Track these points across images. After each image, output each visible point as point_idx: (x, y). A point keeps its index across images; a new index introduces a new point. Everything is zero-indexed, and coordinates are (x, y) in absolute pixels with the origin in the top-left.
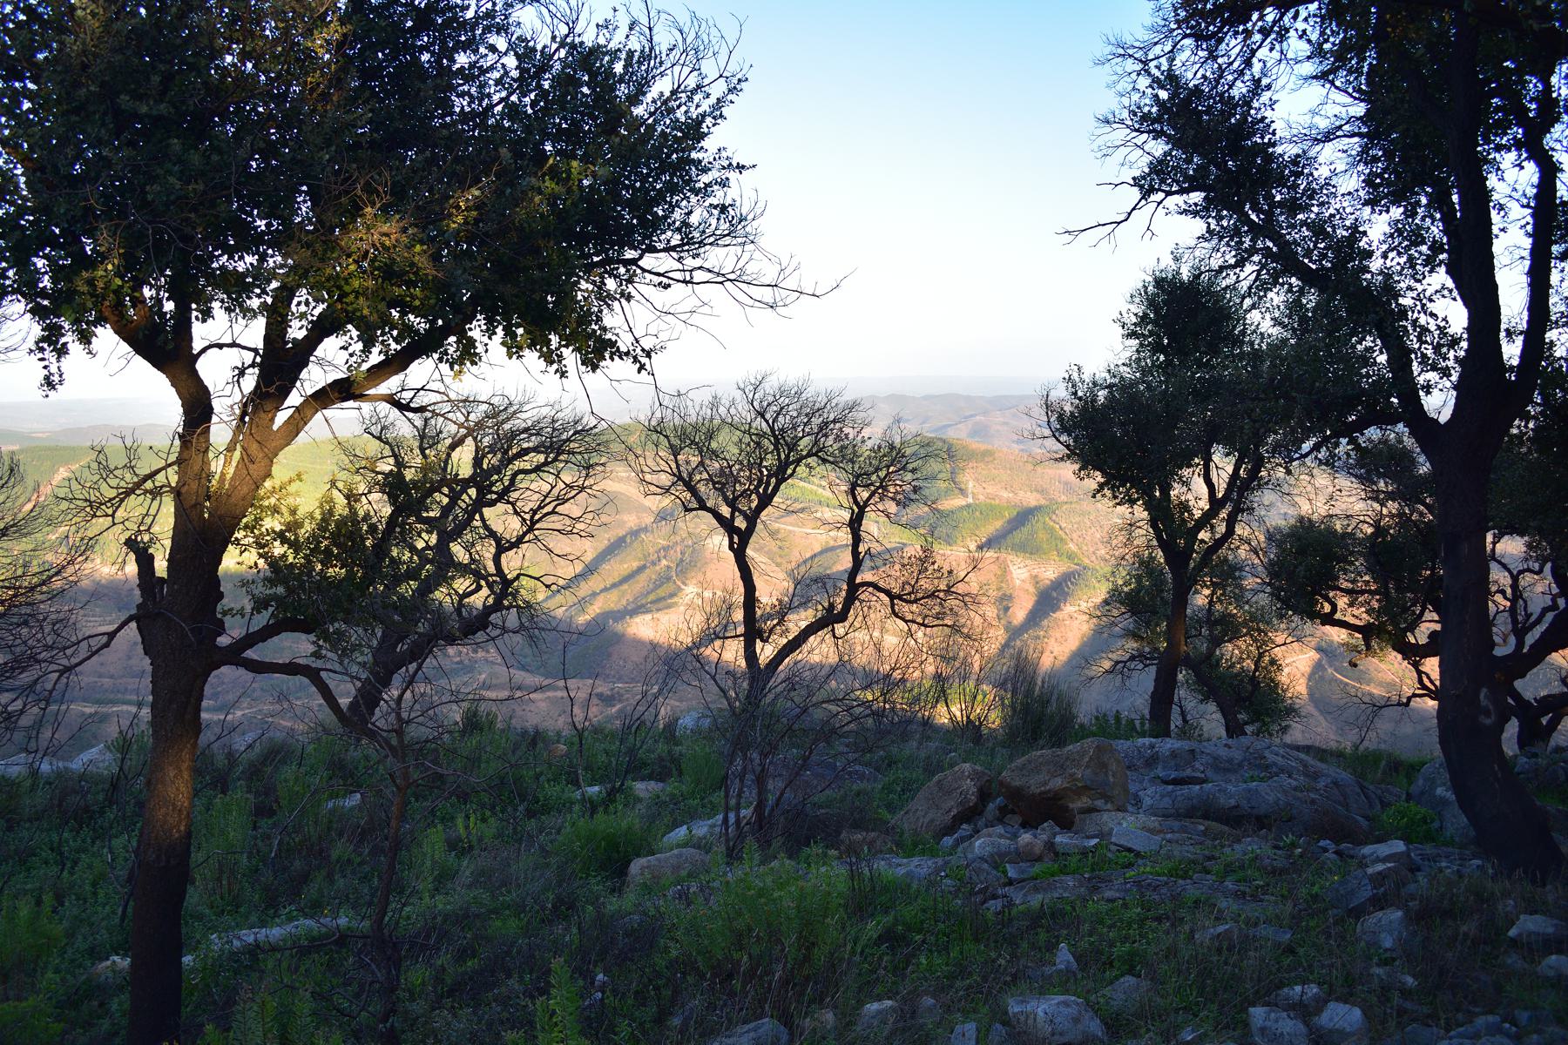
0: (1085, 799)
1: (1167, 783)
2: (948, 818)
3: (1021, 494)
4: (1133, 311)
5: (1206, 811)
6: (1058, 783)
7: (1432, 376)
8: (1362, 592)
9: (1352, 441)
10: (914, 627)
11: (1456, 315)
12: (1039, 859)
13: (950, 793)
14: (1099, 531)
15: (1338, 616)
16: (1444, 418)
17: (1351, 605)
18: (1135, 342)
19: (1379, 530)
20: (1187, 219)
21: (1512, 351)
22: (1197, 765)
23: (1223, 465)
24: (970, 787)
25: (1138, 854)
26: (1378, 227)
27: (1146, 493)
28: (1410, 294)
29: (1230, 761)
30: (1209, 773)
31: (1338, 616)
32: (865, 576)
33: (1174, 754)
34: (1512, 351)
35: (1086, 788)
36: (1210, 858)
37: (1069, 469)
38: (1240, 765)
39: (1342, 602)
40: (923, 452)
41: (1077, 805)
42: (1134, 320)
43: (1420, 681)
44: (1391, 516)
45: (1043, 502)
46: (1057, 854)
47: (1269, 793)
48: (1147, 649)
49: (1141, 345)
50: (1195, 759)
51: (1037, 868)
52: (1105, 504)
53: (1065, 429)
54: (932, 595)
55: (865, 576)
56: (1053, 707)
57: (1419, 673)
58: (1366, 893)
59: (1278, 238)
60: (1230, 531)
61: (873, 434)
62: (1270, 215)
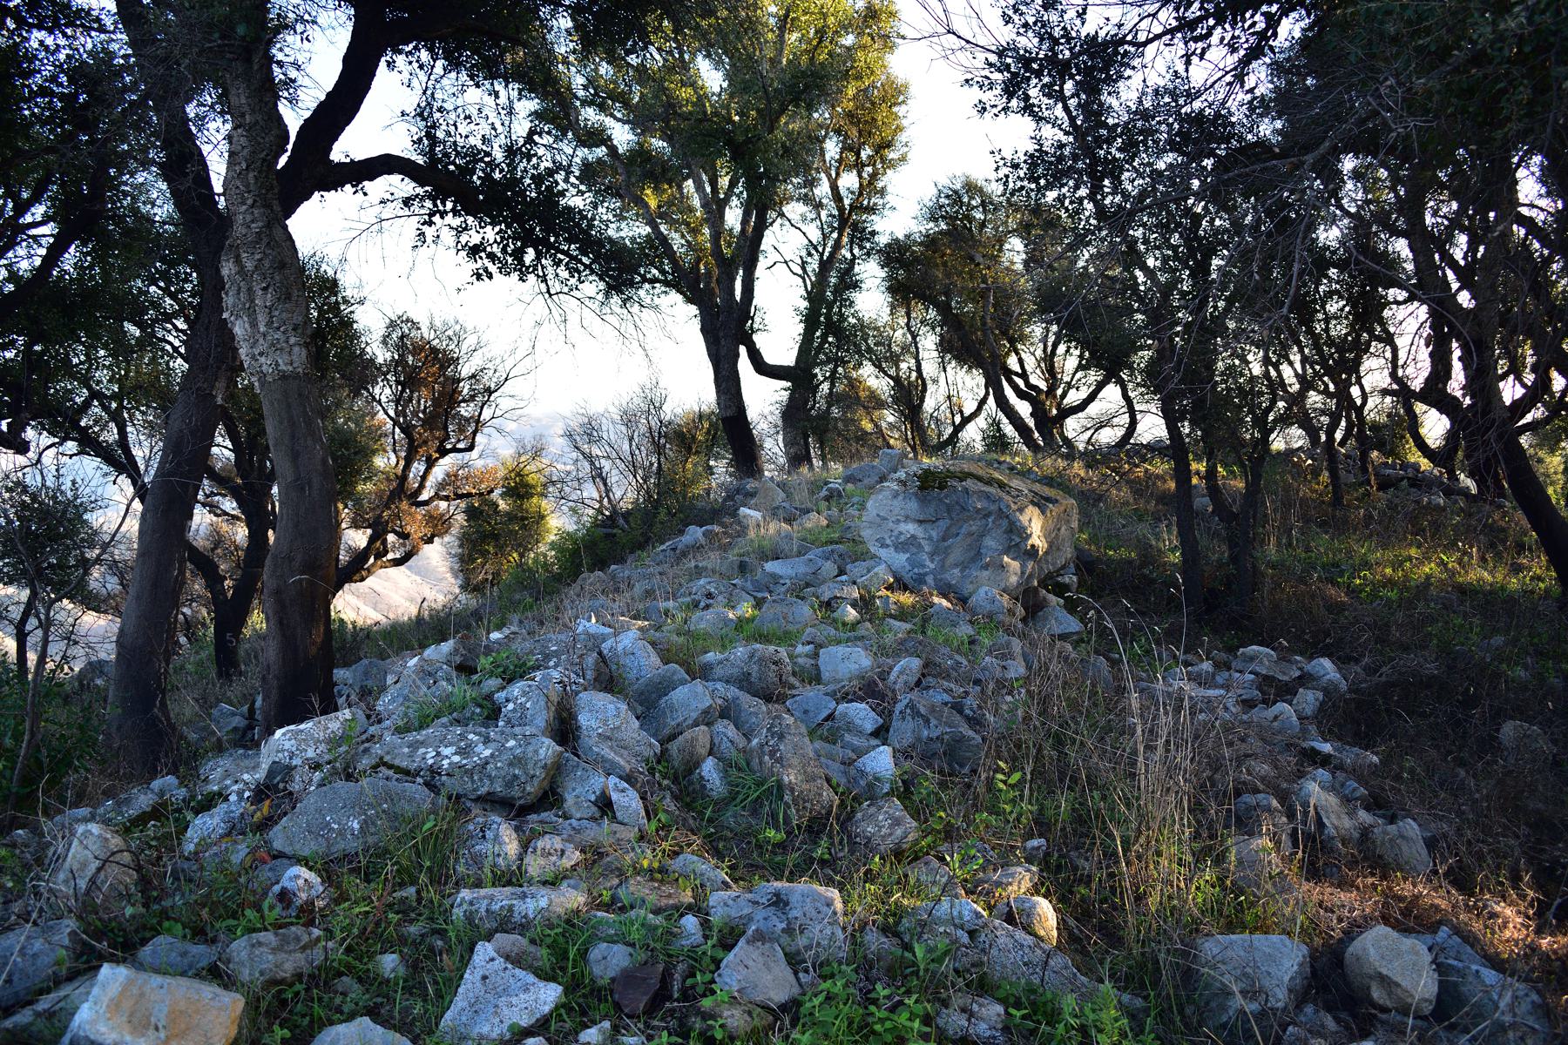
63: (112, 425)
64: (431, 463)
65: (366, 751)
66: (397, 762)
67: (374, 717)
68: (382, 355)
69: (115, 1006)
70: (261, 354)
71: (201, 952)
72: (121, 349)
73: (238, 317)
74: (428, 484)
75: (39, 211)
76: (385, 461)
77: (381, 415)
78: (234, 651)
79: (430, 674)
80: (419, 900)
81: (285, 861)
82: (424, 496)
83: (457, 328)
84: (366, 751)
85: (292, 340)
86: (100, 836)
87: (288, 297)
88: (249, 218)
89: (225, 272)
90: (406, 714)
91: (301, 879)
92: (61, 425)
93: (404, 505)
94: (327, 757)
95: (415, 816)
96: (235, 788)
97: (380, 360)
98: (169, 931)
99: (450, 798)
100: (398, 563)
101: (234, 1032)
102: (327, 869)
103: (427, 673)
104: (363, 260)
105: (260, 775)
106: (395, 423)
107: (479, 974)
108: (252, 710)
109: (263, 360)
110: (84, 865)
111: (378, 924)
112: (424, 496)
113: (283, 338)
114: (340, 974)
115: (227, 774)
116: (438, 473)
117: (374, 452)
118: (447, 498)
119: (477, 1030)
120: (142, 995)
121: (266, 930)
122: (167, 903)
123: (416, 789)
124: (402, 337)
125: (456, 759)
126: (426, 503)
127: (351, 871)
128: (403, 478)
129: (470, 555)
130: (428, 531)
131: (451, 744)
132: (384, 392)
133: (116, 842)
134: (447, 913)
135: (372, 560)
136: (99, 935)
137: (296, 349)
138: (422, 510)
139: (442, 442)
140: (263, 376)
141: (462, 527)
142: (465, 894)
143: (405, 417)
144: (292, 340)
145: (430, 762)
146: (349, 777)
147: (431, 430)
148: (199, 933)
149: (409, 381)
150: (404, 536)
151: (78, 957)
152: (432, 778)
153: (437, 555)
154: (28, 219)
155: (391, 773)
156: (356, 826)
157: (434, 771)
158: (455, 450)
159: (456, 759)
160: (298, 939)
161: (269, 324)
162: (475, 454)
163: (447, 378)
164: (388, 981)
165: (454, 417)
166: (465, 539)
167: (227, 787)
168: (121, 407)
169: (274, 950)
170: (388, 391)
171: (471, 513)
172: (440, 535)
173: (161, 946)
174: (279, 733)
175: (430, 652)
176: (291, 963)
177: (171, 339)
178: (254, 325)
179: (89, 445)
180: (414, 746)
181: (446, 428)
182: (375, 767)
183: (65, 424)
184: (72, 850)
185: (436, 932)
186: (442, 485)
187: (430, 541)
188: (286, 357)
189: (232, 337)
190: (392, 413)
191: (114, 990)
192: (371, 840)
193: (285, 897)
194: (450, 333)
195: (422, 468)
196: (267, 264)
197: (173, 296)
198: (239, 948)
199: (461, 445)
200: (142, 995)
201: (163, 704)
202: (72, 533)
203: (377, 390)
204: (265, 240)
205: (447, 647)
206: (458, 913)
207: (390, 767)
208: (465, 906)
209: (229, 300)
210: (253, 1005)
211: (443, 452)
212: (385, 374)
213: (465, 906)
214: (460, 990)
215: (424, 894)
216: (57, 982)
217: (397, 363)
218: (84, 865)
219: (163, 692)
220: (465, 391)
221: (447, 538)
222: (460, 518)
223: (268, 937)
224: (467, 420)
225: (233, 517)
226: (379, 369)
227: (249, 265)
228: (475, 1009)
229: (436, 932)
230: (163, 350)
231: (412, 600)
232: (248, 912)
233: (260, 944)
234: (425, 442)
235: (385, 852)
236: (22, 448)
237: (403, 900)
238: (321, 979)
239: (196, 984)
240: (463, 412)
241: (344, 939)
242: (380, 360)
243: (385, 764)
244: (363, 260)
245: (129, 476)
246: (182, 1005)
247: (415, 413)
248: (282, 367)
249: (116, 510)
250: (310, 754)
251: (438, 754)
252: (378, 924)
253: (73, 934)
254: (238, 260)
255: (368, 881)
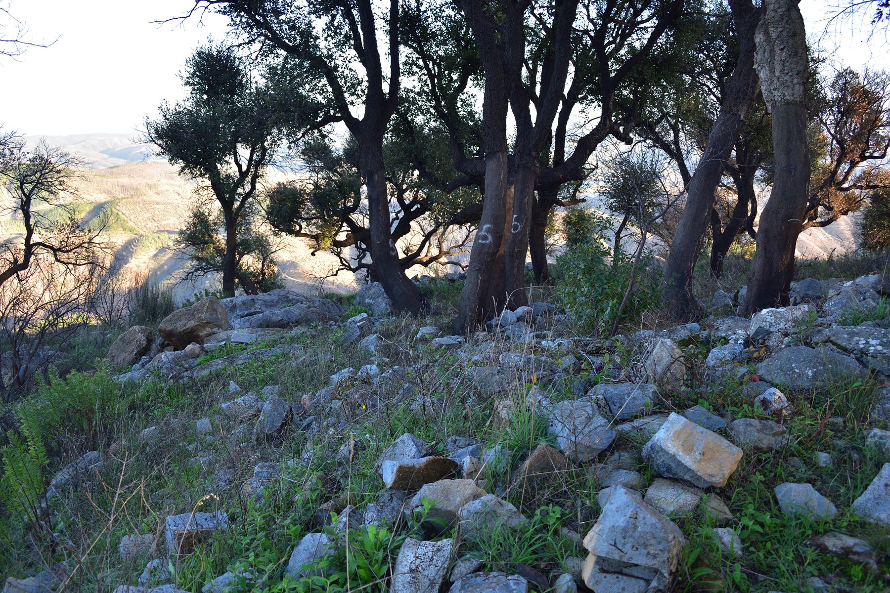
0: (208, 329)
1: (242, 317)
2: (132, 356)
3: (95, 195)
4: (187, 70)
5: (267, 324)
6: (192, 323)
7: (353, 98)
8: (313, 219)
9: (320, 131)
10: (70, 266)
11: (361, 71)
12: (198, 356)
13: (130, 342)
14: (177, 195)
15: (303, 231)
16: (361, 119)
17: (308, 226)
18: (190, 88)
19: (317, 186)
20: (221, 15)
21: (386, 87)
22: (257, 306)
23: (244, 152)
24: (141, 338)
25: (247, 344)
26: (319, 24)
27: (207, 170)
28: (340, 59)
29: (272, 301)
30: (263, 308)
31: (303, 231)
32: (35, 238)
33: (244, 303)
34: (386, 87)
35: (208, 323)
36: (282, 338)
37: (165, 159)
38: (277, 302)
39: (304, 224)
40: (63, 160)
41: (203, 333)
42: (188, 75)
43: (341, 262)
44: (323, 178)
45: (109, 199)
46: (207, 352)
47: (295, 311)
48: (204, 264)
49: (194, 90)
50: (255, 303)
51: (199, 360)
52: (180, 180)
53: (160, 137)
54: (80, 246)
55: (35, 238)
56: (160, 300)
57: (341, 258)
58: (358, 333)
59: (270, 29)
60: (253, 188)
61: (30, 150)
62: (264, 17)
63: (671, 132)
64: (853, 164)
65: (819, 331)
66: (839, 342)
67: (821, 313)
68: (830, 94)
69: (677, 435)
70: (775, 89)
71: (722, 422)
72: (680, 89)
73: (763, 67)
74: (850, 178)
75: (646, 14)
76: (826, 161)
77: (826, 133)
78: (721, 262)
79: (861, 293)
80: (845, 427)
81: (765, 383)
82: (846, 185)
83: (884, 77)
84: (819, 331)
85: (795, 81)
86: (670, 346)
87: (796, 54)
88: (777, 6)
89: (757, 40)
90: (843, 315)
91: (776, 395)
92: (645, 132)
93: (833, 190)
94: (792, 330)
95: (849, 376)
96: (734, 337)
97: (829, 97)
98: (702, 404)
99: (873, 372)
100: (823, 224)
101: (735, 468)
102: (792, 394)
103: (860, 292)
104: (838, 31)
105: (751, 332)
106: (834, 137)
107: (883, 482)
108: (736, 297)
109: (775, 93)
110: (660, 359)
111: (819, 434)
112: (846, 185)
113: (790, 80)
114: (793, 455)
115: (729, 328)
116: (858, 170)
117: (819, 155)
118: (861, 188)
119: (876, 514)
120: (691, 434)
121: (753, 418)
122: (703, 389)
123: (850, 360)
124: (845, 84)
125: (880, 348)
126: (846, 189)
127: (806, 399)
128: (834, 173)
129: (871, 225)
130: (845, 207)
131: (877, 338)
132: (829, 118)
133: (678, 352)
134: (864, 438)
135: (806, 221)
136: (667, 396)
137: (797, 86)
138: (843, 194)
139: (863, 152)
140: (774, 102)
141: (868, 207)
142: (876, 431)
143: (841, 134)
144: (795, 81)
145: (862, 346)
146: (807, 344)
147: (857, 143)
148: (718, 410)
149: (846, 112)
150: (830, 208)
151: (656, 405)
152: (862, 356)
153: (845, 224)
154: (639, 19)
155: (835, 347)
156: (810, 373)
157: (863, 352)
158: (872, 157)
159: (880, 348)
160: (772, 429)
161: (782, 71)
162: (885, 160)
163: (872, 111)
164: (821, 468)
165: (874, 136)
166: (868, 215)
167: (729, 335)
168: (677, 121)
169: (758, 431)
170: (832, 117)
171: (876, 199)
172: (853, 210)
173: (700, 410)
174: (764, 311)
175: (859, 280)
176: (766, 441)
177: (708, 84)
178: (772, 71)
179: (659, 142)
180: (852, 335)
181: (867, 142)
182: (825, 342)
183: (648, 130)
184: (655, 351)
185: (854, 448)
186: (860, 179)
187: (845, 213)
188: (790, 91)
189: (757, 77)
190: (832, 131)
191: (678, 427)
192: (818, 384)
193: (765, 403)
194: (878, 80)
195: (847, 167)
196: (785, 34)
197: (712, 60)
198: (739, 424)
199: (876, 154)
200: (691, 434)
201: (690, 285)
202: (648, 187)
203: (824, 118)
204: (786, 19)
205: (872, 278)
206: (870, 441)
207: (834, 344)
208: (876, 439)
209: (758, 57)
210: (746, 460)
211: (863, 158)
212: (832, 107)
213: (876, 439)
214: (870, 487)
215: (848, 424)
216: (644, 414)
217: (840, 100)
218: (660, 359)
219: (691, 278)
220: (884, 119)
221: (857, 213)
222: (867, 201)
223: (755, 422)
224: (883, 138)
225: (729, 188)
226: (827, 104)
227: (774, 35)
228: (877, 501)
229: (854, 448)
230: (703, 90)
231: (826, 250)
232: (745, 406)
233: (751, 425)
234: (852, 151)
235: (827, 394)
236: (629, 141)
237: (834, 424)
238: (784, 454)
239: (715, 435)
240: (881, 133)
241: (798, 437)
242: (829, 97)
243: (831, 341)
244: (838, 31)
245: (677, 160)
246: (711, 445)
247: (847, 133)
248: (787, 97)
249: (671, 180)
250: (782, 326)
251: (867, 343)
252: (819, 434)
253: (654, 392)
254: (767, 34)
255: (815, 408)
